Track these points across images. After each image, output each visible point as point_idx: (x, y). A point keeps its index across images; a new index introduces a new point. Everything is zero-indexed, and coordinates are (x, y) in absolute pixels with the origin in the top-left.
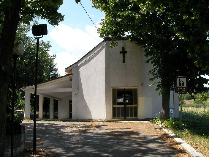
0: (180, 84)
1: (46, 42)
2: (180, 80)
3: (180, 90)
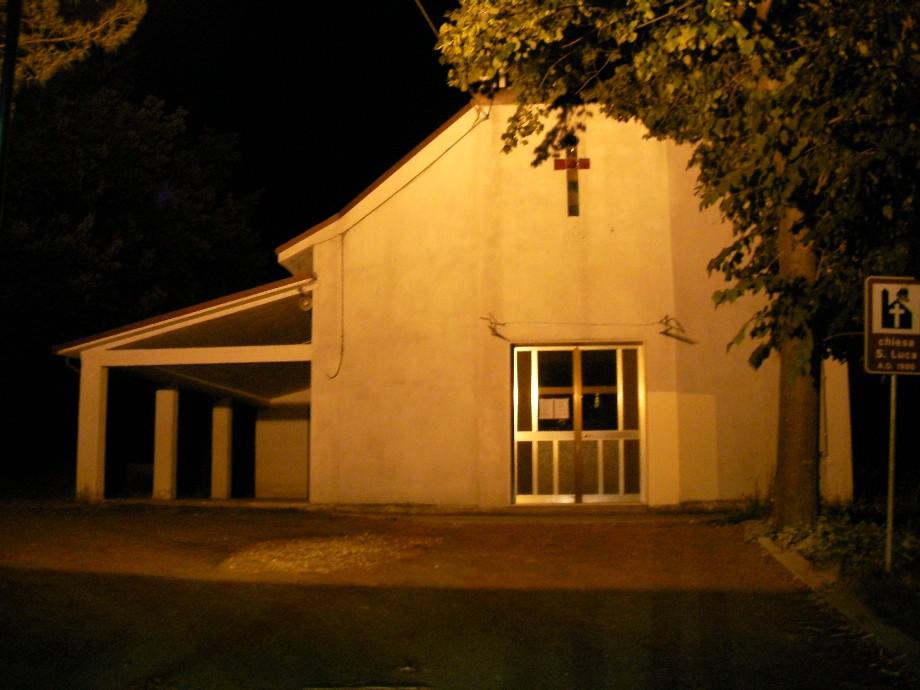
0: (888, 321)
1: (83, 486)
2: (885, 294)
3: (887, 350)
